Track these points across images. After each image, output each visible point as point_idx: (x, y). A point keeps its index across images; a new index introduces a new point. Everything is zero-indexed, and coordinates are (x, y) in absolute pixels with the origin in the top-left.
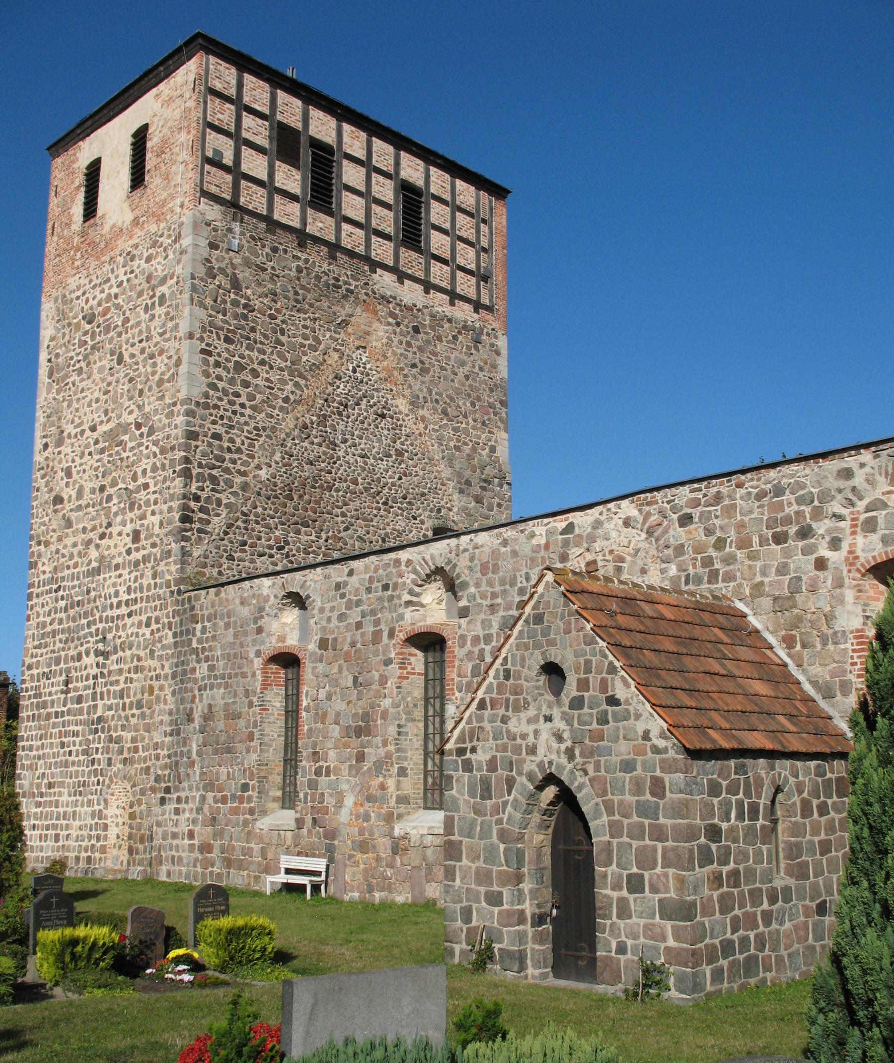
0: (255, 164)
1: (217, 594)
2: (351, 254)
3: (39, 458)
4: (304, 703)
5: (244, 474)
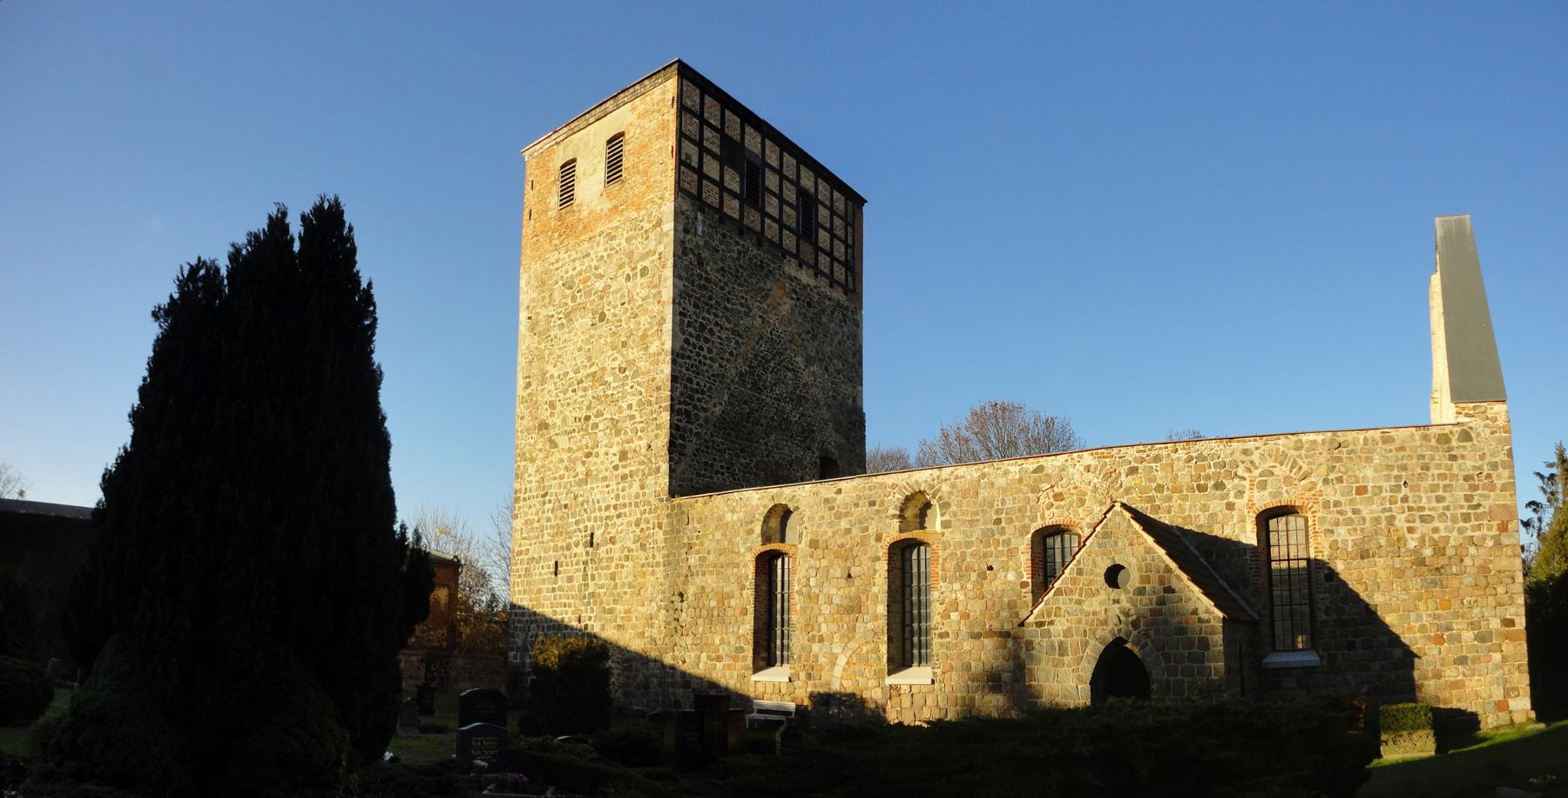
0: (712, 168)
2: (770, 242)
3: (521, 393)
4: (796, 588)
5: (706, 410)
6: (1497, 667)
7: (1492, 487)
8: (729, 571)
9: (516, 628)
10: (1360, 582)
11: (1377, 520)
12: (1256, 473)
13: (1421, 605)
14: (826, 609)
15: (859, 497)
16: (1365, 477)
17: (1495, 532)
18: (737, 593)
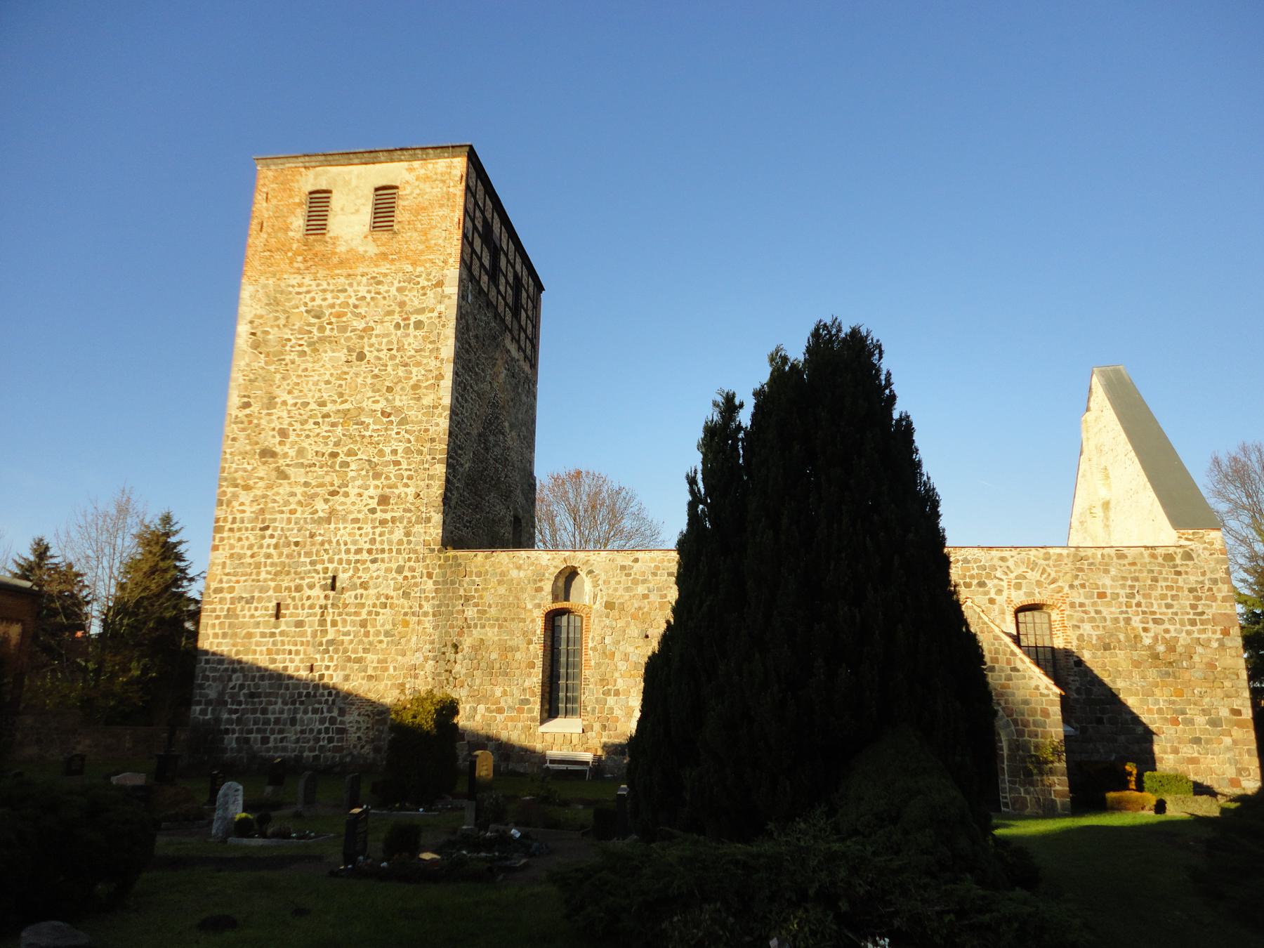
4: (590, 645)
6: (1228, 749)
7: (1214, 599)
8: (514, 625)
9: (206, 678)
10: (1104, 668)
11: (1116, 620)
12: (1012, 576)
13: (1157, 691)
14: (622, 666)
15: (657, 568)
16: (1104, 585)
17: (1219, 636)
18: (523, 646)
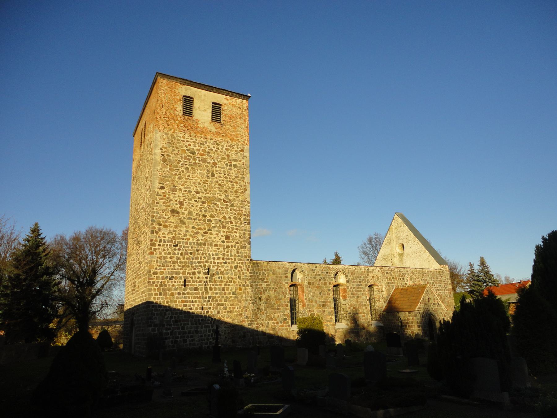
1: (268, 264)
